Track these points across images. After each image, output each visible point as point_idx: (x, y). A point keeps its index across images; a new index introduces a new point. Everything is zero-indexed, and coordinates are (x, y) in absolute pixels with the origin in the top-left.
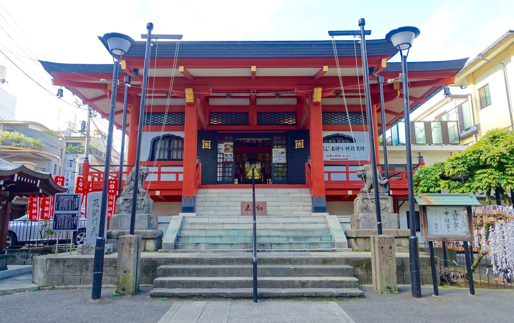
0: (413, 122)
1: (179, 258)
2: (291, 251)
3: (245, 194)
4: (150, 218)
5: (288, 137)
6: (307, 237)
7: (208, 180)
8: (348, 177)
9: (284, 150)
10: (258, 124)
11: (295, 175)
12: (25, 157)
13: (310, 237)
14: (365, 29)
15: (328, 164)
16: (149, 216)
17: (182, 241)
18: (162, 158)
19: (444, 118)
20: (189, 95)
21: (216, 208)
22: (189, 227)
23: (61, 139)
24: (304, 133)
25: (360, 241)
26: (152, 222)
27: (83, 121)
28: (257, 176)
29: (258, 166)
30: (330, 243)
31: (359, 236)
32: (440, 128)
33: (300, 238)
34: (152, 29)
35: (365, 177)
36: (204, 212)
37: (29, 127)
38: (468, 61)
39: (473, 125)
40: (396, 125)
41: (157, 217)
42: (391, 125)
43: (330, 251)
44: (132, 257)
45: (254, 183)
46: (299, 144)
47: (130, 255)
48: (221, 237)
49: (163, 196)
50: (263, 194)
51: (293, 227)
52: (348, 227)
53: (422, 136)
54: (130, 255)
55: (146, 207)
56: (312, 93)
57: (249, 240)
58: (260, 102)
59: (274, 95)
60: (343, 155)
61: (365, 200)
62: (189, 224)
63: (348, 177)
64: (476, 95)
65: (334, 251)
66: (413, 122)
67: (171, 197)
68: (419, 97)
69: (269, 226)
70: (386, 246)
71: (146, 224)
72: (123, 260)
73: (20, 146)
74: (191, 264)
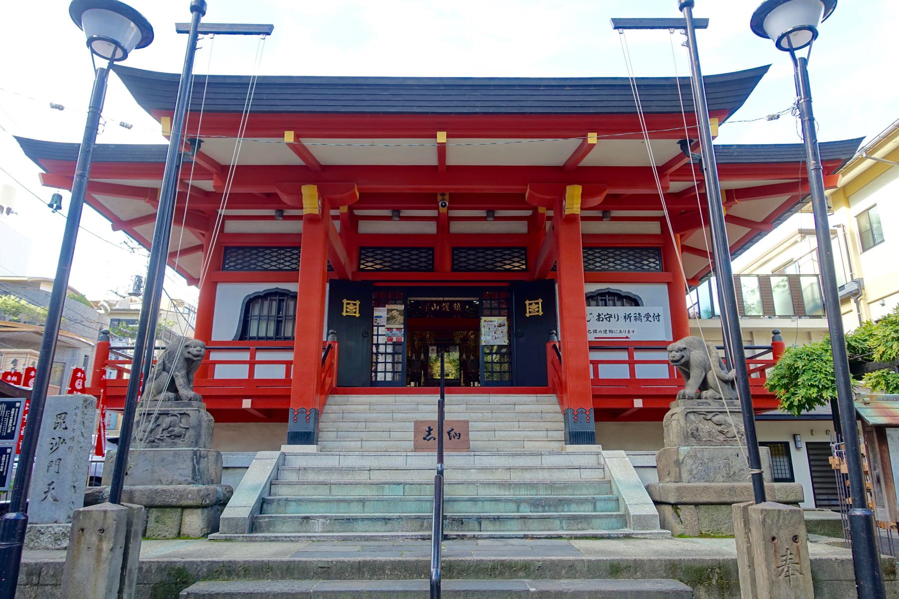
0: (738, 277)
1: (245, 562)
2: (525, 537)
3: (422, 406)
4: (197, 458)
5: (509, 298)
6: (561, 502)
7: (358, 379)
8: (632, 372)
9: (503, 320)
10: (453, 270)
11: (529, 369)
12: (16, 341)
13: (569, 502)
14: (695, 16)
15: (596, 346)
16: (195, 453)
17: (272, 512)
18: (262, 334)
19: (791, 270)
20: (310, 200)
21: (364, 435)
22: (293, 477)
23: (102, 312)
24: (544, 288)
25: (685, 511)
26: (201, 466)
27: (137, 276)
28: (452, 371)
29: (456, 355)
30: (617, 516)
31: (684, 500)
32: (787, 287)
33: (549, 504)
34: (204, 14)
35: (687, 364)
36: (336, 444)
37: (41, 288)
38: (863, 144)
39: (849, 280)
40: (706, 283)
41: (219, 455)
42: (700, 280)
43: (618, 538)
44: (105, 567)
45: (444, 386)
46: (534, 308)
47: (98, 560)
48: (363, 501)
49: (258, 410)
50: (461, 406)
51: (528, 477)
52: (653, 477)
53: (755, 303)
54: (98, 560)
55: (191, 432)
56: (562, 195)
57: (428, 510)
58: (456, 228)
59: (485, 215)
60: (618, 328)
61: (692, 416)
62: (293, 470)
63: (632, 372)
64: (853, 227)
65: (628, 537)
66: (738, 277)
67: (268, 412)
68: (760, 220)
69: (475, 476)
70: (784, 536)
71: (189, 472)
72: (78, 575)
73: (18, 321)
74: (275, 577)
